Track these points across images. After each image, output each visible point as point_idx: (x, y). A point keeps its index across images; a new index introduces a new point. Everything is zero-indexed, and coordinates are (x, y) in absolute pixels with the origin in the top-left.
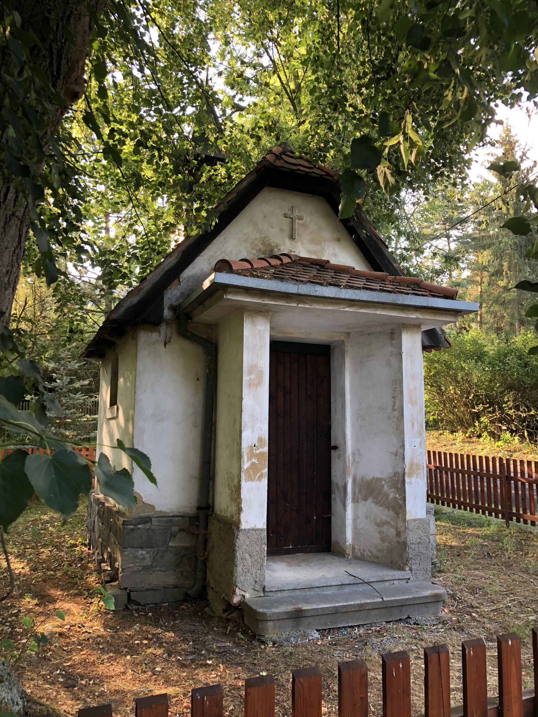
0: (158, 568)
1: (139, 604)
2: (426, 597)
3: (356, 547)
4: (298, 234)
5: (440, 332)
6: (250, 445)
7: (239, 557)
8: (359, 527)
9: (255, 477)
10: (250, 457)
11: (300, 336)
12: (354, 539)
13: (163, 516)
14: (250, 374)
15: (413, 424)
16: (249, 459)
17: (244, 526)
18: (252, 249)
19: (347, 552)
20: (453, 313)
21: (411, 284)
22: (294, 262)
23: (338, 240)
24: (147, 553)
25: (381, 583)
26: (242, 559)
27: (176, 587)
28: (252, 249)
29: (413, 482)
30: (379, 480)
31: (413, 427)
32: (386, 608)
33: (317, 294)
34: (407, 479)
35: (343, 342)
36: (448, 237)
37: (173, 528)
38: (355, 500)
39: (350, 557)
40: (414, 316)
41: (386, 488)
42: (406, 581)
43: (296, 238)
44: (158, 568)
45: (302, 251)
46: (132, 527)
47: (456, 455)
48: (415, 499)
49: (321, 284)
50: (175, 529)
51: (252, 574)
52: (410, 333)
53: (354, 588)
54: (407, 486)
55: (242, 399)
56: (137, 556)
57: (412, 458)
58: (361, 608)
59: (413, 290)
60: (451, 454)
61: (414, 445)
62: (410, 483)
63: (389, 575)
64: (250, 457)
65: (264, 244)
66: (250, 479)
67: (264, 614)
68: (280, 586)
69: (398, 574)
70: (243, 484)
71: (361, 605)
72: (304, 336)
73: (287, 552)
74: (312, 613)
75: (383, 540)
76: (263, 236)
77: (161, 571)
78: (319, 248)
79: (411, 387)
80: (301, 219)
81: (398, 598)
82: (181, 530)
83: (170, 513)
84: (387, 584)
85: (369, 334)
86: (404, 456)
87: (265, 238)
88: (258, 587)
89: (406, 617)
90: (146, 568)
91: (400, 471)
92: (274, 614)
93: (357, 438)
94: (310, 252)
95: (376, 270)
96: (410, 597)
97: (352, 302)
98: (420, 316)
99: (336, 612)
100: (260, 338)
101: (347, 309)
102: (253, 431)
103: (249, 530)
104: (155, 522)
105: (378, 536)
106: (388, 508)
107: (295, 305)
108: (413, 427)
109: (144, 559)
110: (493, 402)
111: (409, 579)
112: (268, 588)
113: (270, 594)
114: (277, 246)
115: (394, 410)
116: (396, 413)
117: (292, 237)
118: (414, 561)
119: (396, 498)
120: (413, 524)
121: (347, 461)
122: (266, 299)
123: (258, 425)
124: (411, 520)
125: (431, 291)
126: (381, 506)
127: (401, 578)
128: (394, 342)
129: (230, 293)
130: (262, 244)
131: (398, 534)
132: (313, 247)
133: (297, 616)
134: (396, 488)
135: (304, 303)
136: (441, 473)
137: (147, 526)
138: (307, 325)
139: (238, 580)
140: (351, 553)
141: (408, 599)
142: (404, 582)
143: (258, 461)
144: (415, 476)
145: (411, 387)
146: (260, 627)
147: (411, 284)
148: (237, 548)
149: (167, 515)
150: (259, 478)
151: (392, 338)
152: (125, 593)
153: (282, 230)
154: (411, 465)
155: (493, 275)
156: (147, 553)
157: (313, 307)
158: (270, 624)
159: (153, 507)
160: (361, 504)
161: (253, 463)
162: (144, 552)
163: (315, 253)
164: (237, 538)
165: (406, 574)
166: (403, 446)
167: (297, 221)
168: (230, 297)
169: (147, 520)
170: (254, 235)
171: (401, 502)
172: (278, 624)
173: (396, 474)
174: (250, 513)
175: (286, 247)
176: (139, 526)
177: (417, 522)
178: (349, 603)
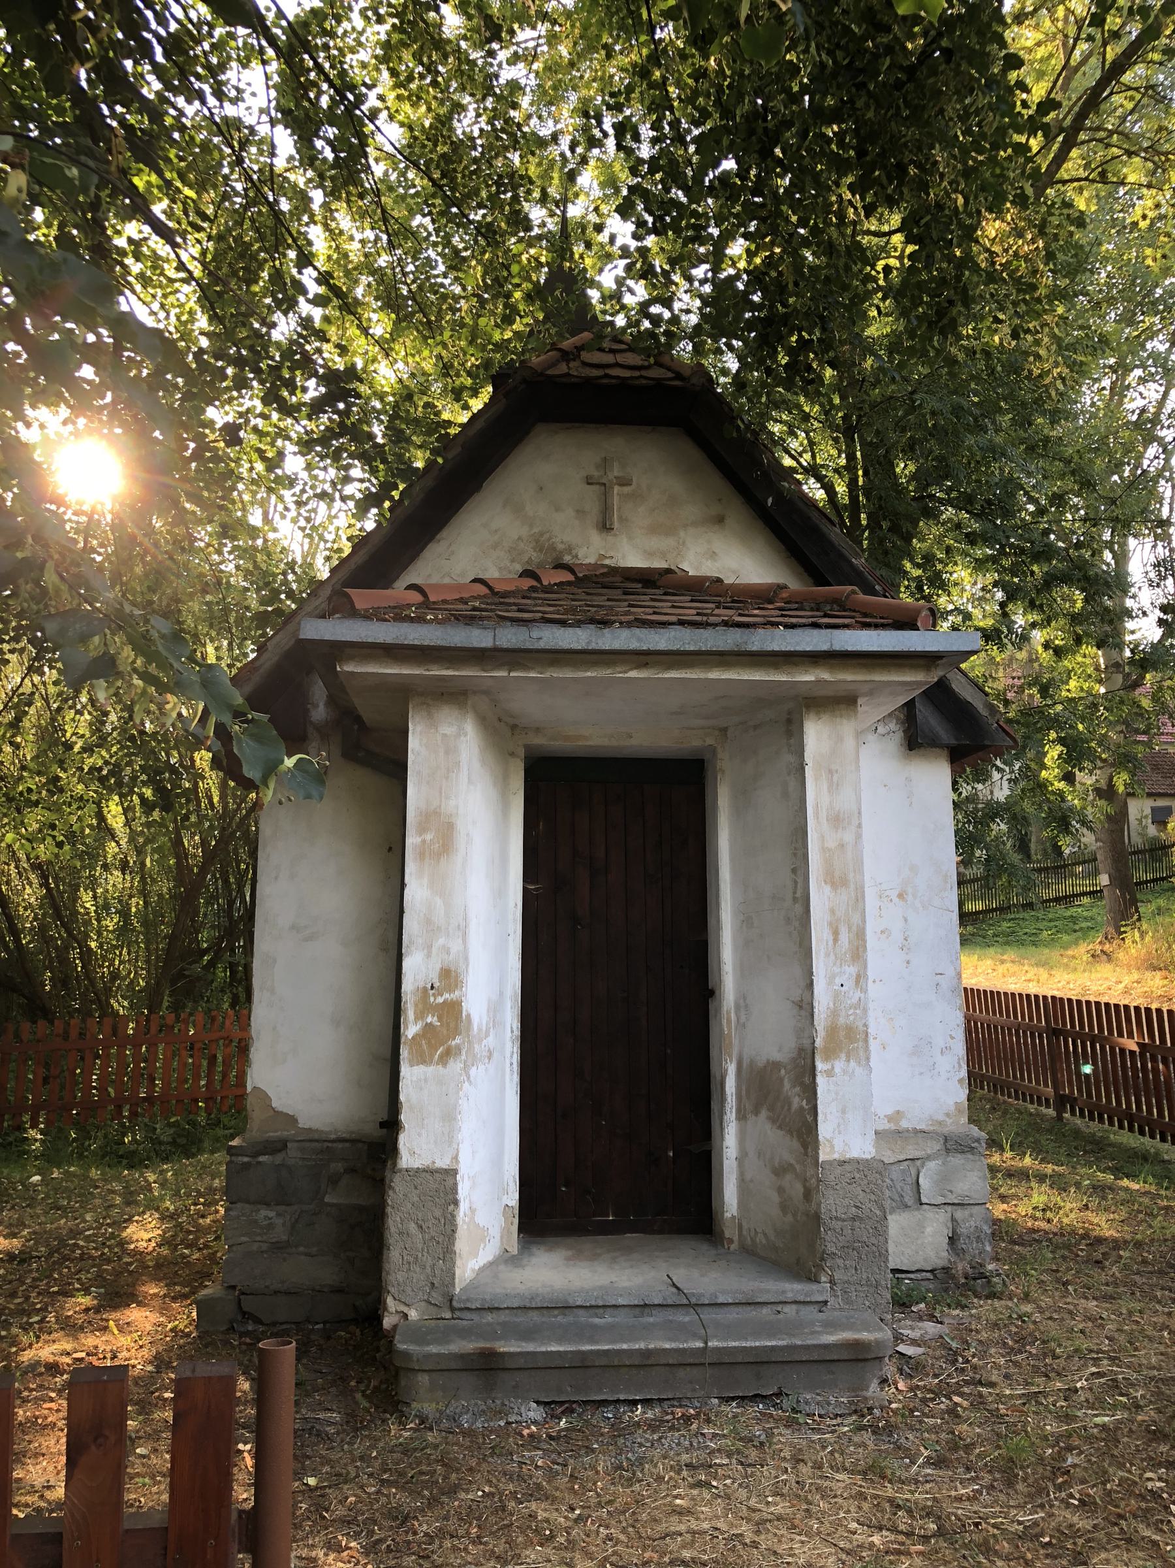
0: (301, 1249)
1: (258, 1321)
2: (826, 1347)
3: (744, 1224)
4: (620, 518)
5: (984, 712)
6: (421, 985)
7: (393, 1229)
8: (748, 1177)
9: (432, 1056)
10: (422, 1013)
11: (605, 742)
14: (422, 830)
15: (836, 934)
16: (419, 1016)
17: (406, 1160)
18: (513, 561)
19: (727, 1235)
20: (922, 662)
21: (826, 602)
22: (580, 582)
23: (720, 520)
24: (278, 1215)
25: (749, 1308)
26: (400, 1233)
27: (339, 1291)
28: (513, 561)
29: (837, 1070)
30: (776, 1065)
31: (836, 940)
32: (725, 1365)
33: (542, 645)
34: (820, 1065)
35: (713, 750)
37: (333, 1165)
38: (741, 1116)
39: (733, 1247)
40: (809, 677)
41: (787, 1085)
42: (817, 1307)
43: (616, 525)
44: (301, 1249)
45: (631, 554)
46: (246, 1159)
47: (1148, 1010)
48: (844, 1112)
49: (563, 623)
50: (338, 1167)
51: (424, 1267)
52: (825, 717)
53: (670, 1315)
54: (820, 1080)
55: (403, 885)
56: (256, 1221)
57: (834, 1013)
58: (646, 1362)
59: (826, 615)
61: (838, 981)
62: (830, 1073)
63: (768, 1291)
64: (422, 1013)
65: (539, 548)
66: (422, 1059)
67: (406, 1355)
68: (488, 1297)
69: (794, 1289)
70: (405, 1070)
71: (647, 1353)
72: (614, 743)
73: (605, 1229)
74: (521, 1363)
75: (784, 1207)
76: (536, 530)
77: (306, 1254)
79: (831, 844)
80: (624, 482)
81: (748, 1344)
82: (351, 1171)
83: (330, 1132)
84: (765, 1311)
85: (755, 727)
86: (812, 1007)
87: (542, 534)
88: (436, 1298)
89: (776, 1390)
90: (278, 1247)
91: (806, 1042)
92: (429, 1356)
93: (743, 971)
94: (650, 554)
95: (821, 581)
96: (784, 1343)
98: (826, 676)
99: (582, 1364)
100: (447, 752)
101: (633, 674)
102: (429, 956)
103: (418, 1170)
104: (293, 1151)
105: (776, 1198)
106: (790, 1132)
107: (505, 674)
108: (836, 940)
109: (271, 1226)
111: (826, 1302)
112: (460, 1301)
113: (467, 1315)
114: (569, 550)
115: (795, 900)
116: (798, 908)
117: (605, 527)
118: (840, 1262)
119: (801, 1108)
120: (839, 1170)
121: (724, 1022)
122: (435, 667)
123: (441, 941)
124: (830, 1163)
125: (865, 615)
126: (780, 1128)
127: (801, 1298)
128: (792, 741)
129: (351, 658)
130: (534, 549)
131: (808, 1195)
133: (487, 1368)
134: (802, 1084)
135: (525, 668)
136: (1154, 1059)
137: (278, 1158)
138: (614, 711)
139: (392, 1278)
140: (736, 1238)
141: (773, 1348)
142: (813, 1309)
143: (440, 1019)
144: (843, 1056)
145: (831, 844)
146: (403, 1383)
147: (826, 602)
148: (389, 1210)
149: (324, 1137)
150: (441, 1057)
151: (789, 734)
153: (580, 513)
154: (832, 1031)
156: (278, 1215)
157: (547, 675)
158: (424, 1379)
159: (292, 1120)
160: (752, 1118)
161: (428, 1026)
162: (272, 1214)
163: (663, 555)
164: (390, 1187)
165: (819, 1291)
166: (811, 984)
167: (616, 489)
168: (349, 668)
169: (281, 1146)
171: (810, 1119)
173: (801, 1050)
174: (419, 1135)
175: (591, 549)
176: (261, 1159)
177: (847, 1167)
178: (617, 1347)
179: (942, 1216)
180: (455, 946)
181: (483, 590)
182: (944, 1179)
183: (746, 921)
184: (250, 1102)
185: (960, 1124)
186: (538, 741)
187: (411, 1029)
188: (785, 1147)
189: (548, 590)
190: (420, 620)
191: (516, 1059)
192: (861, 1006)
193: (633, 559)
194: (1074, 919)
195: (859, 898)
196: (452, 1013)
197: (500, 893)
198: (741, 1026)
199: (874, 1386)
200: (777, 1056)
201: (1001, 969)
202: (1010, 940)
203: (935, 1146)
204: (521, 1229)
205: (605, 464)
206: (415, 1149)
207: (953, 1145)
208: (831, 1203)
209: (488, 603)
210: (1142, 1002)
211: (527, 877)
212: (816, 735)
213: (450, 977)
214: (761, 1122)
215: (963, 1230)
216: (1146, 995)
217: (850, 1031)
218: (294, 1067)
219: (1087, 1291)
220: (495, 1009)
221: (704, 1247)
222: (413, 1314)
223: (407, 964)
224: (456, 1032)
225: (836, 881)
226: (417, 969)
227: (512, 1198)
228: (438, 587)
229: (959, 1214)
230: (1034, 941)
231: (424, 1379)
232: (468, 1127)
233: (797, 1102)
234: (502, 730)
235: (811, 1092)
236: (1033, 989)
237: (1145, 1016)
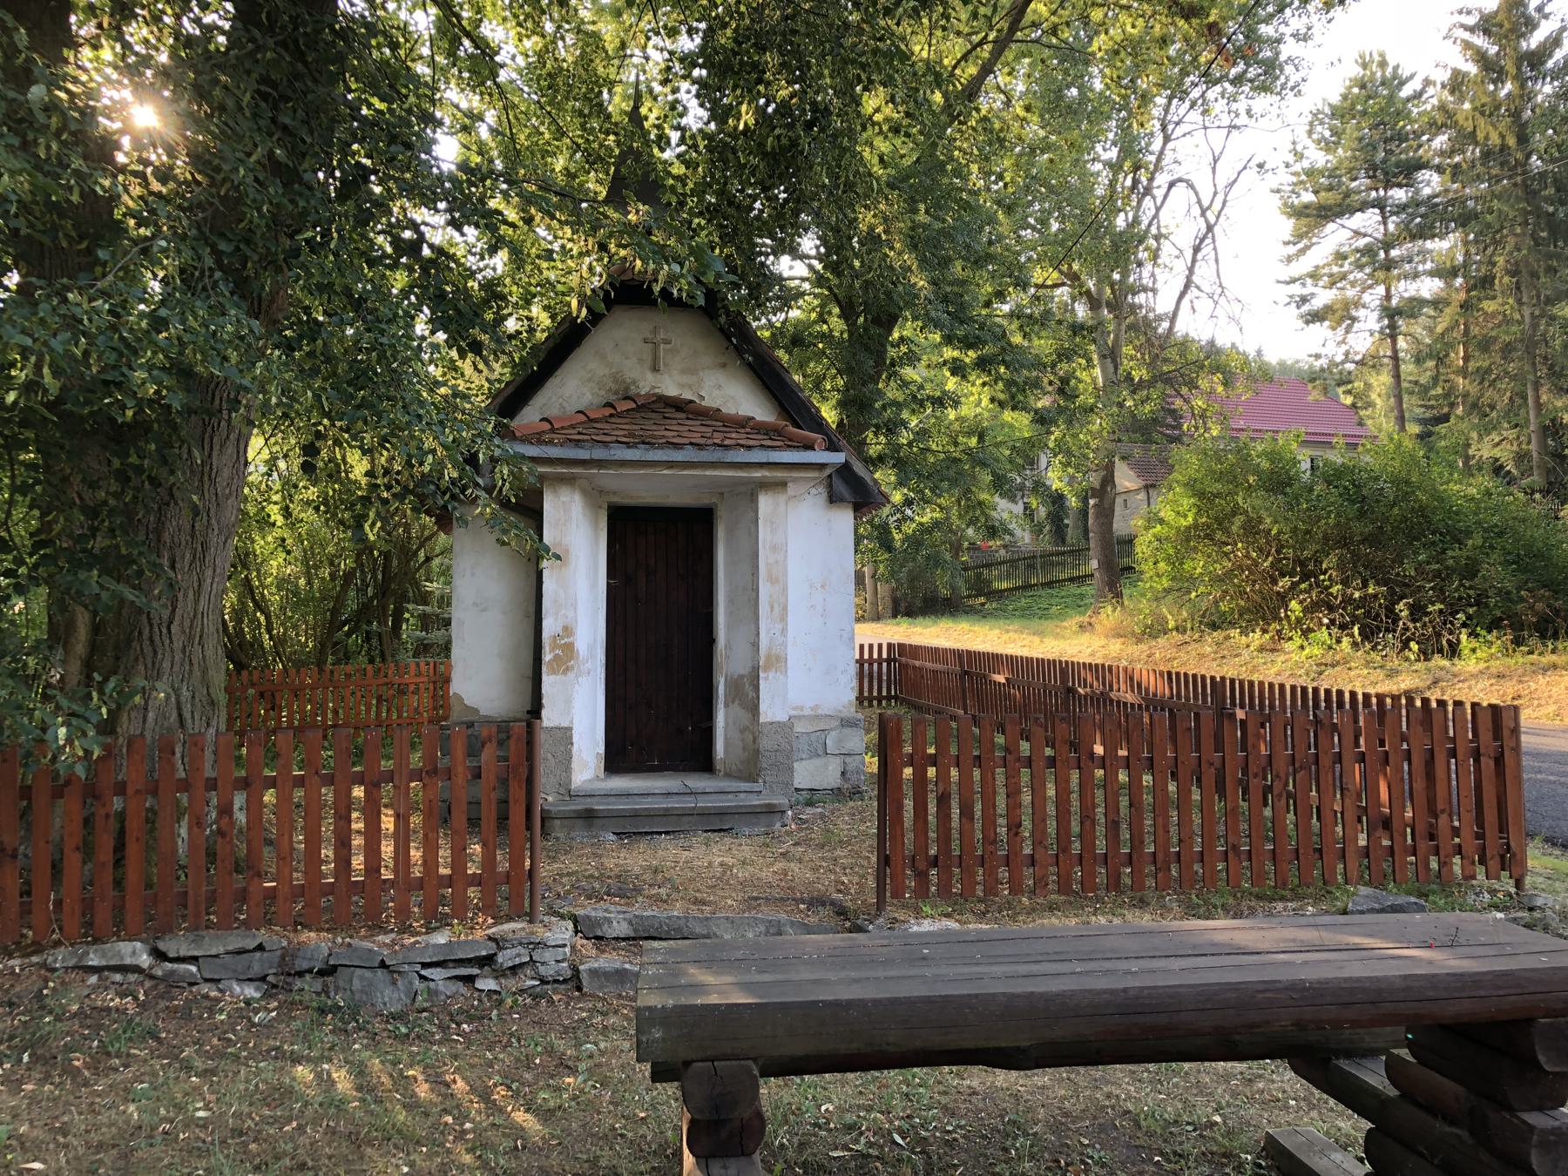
5: (871, 483)
12: (726, 751)
13: (488, 721)
22: (639, 408)
23: (724, 366)
30: (742, 677)
32: (704, 814)
36: (1380, 205)
38: (726, 705)
45: (670, 387)
58: (666, 814)
60: (1203, 677)
62: (766, 679)
65: (616, 381)
66: (553, 672)
70: (544, 677)
78: (695, 378)
79: (771, 561)
93: (729, 627)
97: (671, 464)
98: (767, 474)
110: (1307, 571)
132: (685, 379)
133: (589, 816)
138: (660, 482)
152: (444, 806)
153: (640, 360)
154: (768, 657)
155: (1474, 287)
159: (477, 711)
170: (602, 371)
172: (566, 822)
175: (648, 383)
179: (838, 760)
180: (571, 614)
181: (584, 418)
182: (840, 741)
183: (731, 601)
184: (452, 701)
185: (851, 711)
186: (616, 500)
187: (547, 657)
188: (743, 716)
189: (619, 415)
190: (551, 442)
191: (603, 676)
192: (784, 645)
193: (671, 390)
194: (1082, 596)
195: (785, 590)
196: (570, 647)
197: (594, 585)
198: (728, 657)
199: (778, 825)
200: (742, 672)
201: (1005, 637)
202: (1026, 614)
203: (837, 723)
204: (606, 769)
205: (655, 330)
206: (550, 717)
207: (846, 723)
208: (765, 744)
209: (587, 426)
210: (1099, 661)
211: (609, 577)
212: (765, 502)
213: (568, 631)
214: (736, 709)
215: (849, 768)
216: (1105, 656)
217: (778, 658)
218: (478, 679)
219: (1104, 913)
220: (591, 648)
221: (707, 775)
222: (550, 799)
223: (545, 623)
224: (572, 658)
225: (773, 580)
226: (549, 627)
227: (601, 749)
228: (558, 419)
229: (848, 760)
230: (1045, 615)
231: (558, 822)
232: (578, 707)
233: (751, 694)
234: (593, 495)
235: (757, 688)
236: (1025, 653)
237: (1011, 660)
